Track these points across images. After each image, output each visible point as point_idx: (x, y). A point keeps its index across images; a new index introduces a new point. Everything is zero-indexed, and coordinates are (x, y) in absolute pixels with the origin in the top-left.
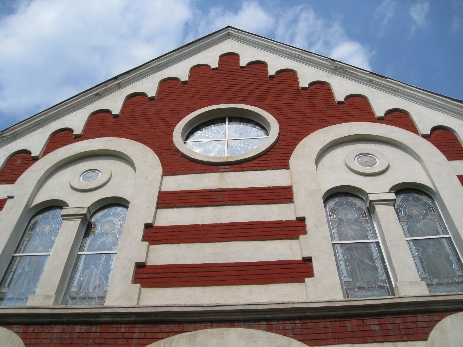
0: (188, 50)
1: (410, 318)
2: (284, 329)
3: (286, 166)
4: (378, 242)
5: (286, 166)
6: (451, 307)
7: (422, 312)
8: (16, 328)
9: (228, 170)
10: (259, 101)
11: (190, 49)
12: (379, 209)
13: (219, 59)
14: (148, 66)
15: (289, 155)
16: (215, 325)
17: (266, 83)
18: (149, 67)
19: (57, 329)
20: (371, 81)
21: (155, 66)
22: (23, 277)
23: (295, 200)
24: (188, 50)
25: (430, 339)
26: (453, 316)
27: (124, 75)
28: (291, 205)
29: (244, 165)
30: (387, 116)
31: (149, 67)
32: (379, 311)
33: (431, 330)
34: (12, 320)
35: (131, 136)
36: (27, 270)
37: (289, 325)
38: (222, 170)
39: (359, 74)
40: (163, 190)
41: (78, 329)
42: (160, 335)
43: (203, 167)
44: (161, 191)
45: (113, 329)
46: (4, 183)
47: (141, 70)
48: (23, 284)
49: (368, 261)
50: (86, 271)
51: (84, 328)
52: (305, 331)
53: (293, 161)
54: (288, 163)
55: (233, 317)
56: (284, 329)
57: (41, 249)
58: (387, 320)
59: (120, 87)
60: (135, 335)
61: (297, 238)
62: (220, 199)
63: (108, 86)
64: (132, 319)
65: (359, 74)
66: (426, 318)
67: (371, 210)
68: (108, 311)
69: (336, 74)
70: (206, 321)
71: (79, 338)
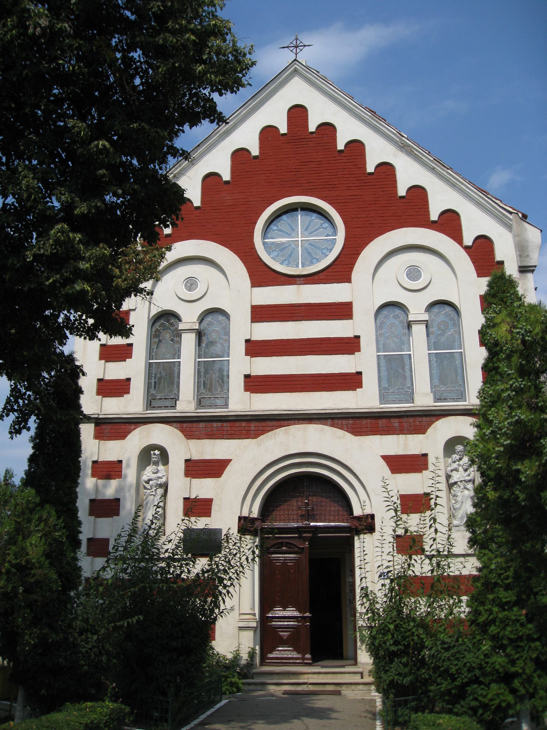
0: (254, 103)
1: (419, 419)
2: (342, 424)
3: (348, 280)
4: (410, 355)
5: (348, 280)
6: (444, 413)
7: (426, 416)
8: (175, 424)
9: (302, 282)
10: (327, 189)
11: (257, 101)
12: (415, 328)
13: (288, 115)
14: (217, 133)
15: (352, 266)
16: (300, 422)
17: (334, 162)
18: (218, 135)
19: (202, 425)
20: (434, 169)
21: (224, 132)
22: (163, 381)
23: (354, 318)
24: (254, 103)
25: (427, 433)
26: (444, 419)
27: (195, 150)
28: (350, 284)
29: (316, 277)
30: (441, 218)
31: (218, 135)
32: (400, 414)
33: (428, 428)
34: (171, 420)
35: (216, 236)
36: (164, 374)
37: (344, 422)
38: (298, 282)
39: (423, 158)
40: (254, 304)
41: (215, 425)
42: (267, 428)
43: (284, 278)
44: (253, 304)
45: (238, 424)
46: (176, 371)
47: (211, 139)
48: (164, 386)
49: (400, 370)
50: (207, 376)
51: (219, 424)
52: (354, 426)
53: (355, 275)
54: (350, 275)
55: (311, 417)
56: (342, 424)
57: (168, 355)
58: (404, 420)
59: (193, 164)
60: (252, 428)
61: (354, 354)
62: (298, 315)
63: (182, 166)
64: (249, 418)
65: (423, 158)
66: (428, 419)
67: (409, 325)
68: (233, 414)
69: (402, 152)
70: (295, 419)
71: (217, 430)
